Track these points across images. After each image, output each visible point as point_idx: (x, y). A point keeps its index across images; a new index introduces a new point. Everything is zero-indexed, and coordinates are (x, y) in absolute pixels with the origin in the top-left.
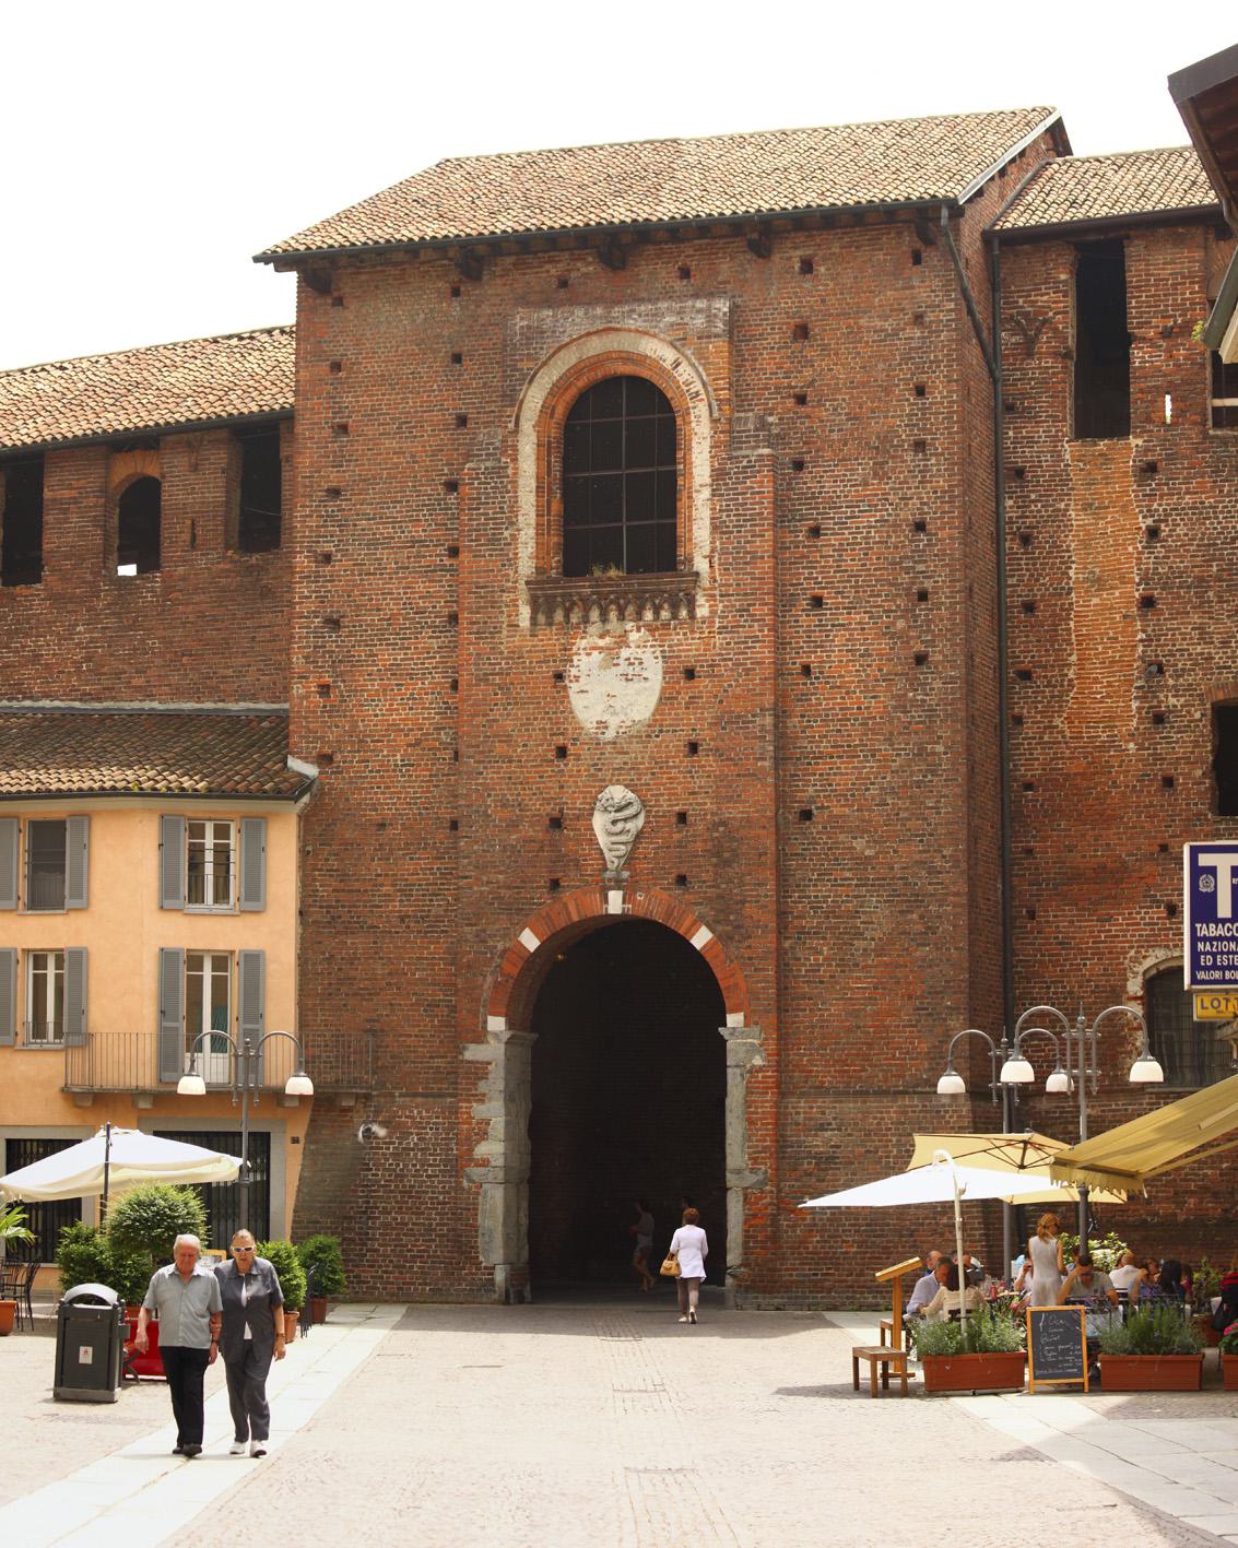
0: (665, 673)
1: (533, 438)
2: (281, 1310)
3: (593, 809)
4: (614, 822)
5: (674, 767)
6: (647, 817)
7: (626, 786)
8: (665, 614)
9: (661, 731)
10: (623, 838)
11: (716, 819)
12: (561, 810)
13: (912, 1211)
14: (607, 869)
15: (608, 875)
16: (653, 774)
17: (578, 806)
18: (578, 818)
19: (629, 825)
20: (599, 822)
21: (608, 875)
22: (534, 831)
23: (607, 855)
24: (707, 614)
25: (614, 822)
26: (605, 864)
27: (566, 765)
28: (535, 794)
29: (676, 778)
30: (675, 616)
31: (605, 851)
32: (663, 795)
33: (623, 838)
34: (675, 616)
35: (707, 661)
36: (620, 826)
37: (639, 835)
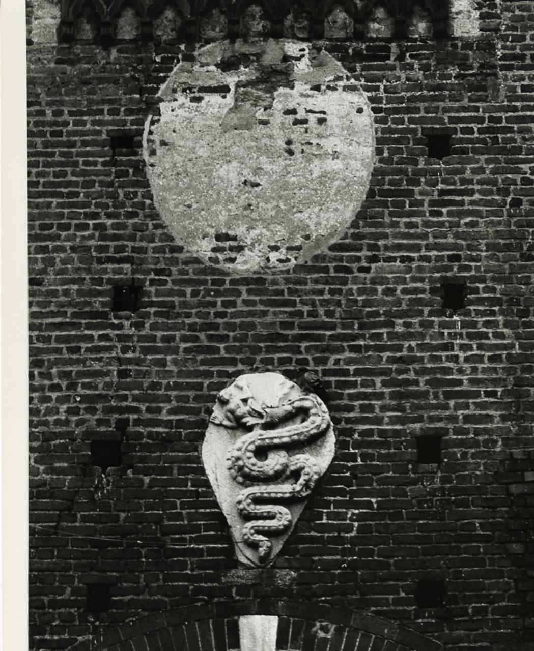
0: (379, 141)
1: (72, 285)
2: (87, 405)
3: (204, 425)
4: (261, 452)
5: (410, 336)
6: (340, 445)
7: (288, 374)
8: (378, 28)
9: (374, 259)
10: (285, 489)
11: (517, 452)
12: (122, 425)
13: (254, 612)
14: (236, 564)
15: (239, 576)
16: (356, 349)
17: (164, 416)
18: (166, 442)
19: (301, 459)
20: (218, 453)
21: (239, 576)
22: (51, 470)
23: (240, 530)
24: (476, 33)
25: (261, 452)
26: (230, 552)
27: (139, 326)
28: (55, 388)
29: (414, 360)
30: (401, 33)
31: (232, 519)
32: (379, 396)
33: (285, 489)
34: (401, 33)
35: (481, 120)
36: (274, 462)
37: (325, 482)
